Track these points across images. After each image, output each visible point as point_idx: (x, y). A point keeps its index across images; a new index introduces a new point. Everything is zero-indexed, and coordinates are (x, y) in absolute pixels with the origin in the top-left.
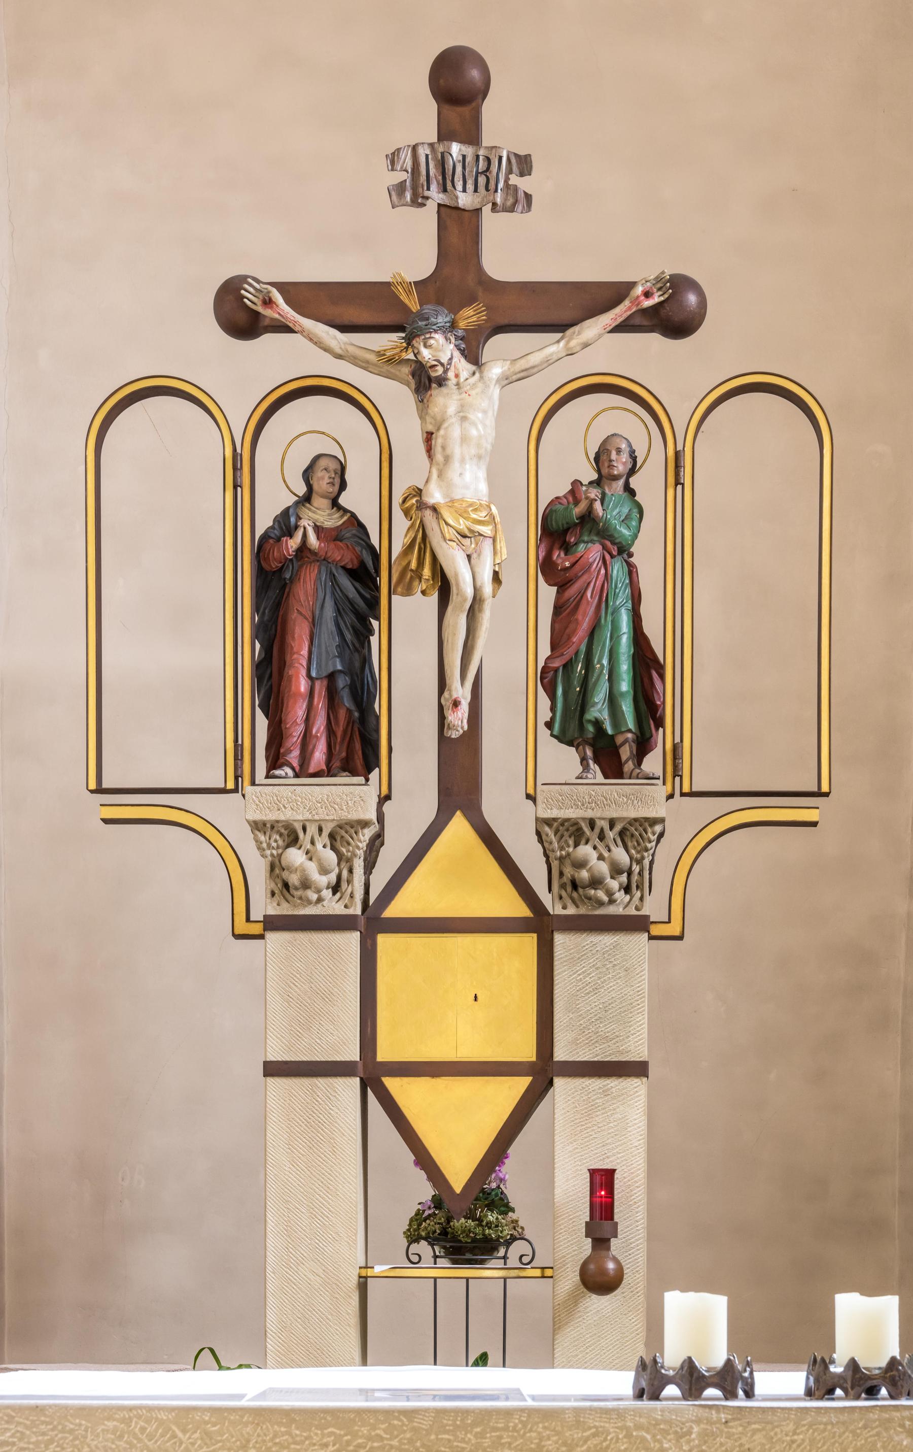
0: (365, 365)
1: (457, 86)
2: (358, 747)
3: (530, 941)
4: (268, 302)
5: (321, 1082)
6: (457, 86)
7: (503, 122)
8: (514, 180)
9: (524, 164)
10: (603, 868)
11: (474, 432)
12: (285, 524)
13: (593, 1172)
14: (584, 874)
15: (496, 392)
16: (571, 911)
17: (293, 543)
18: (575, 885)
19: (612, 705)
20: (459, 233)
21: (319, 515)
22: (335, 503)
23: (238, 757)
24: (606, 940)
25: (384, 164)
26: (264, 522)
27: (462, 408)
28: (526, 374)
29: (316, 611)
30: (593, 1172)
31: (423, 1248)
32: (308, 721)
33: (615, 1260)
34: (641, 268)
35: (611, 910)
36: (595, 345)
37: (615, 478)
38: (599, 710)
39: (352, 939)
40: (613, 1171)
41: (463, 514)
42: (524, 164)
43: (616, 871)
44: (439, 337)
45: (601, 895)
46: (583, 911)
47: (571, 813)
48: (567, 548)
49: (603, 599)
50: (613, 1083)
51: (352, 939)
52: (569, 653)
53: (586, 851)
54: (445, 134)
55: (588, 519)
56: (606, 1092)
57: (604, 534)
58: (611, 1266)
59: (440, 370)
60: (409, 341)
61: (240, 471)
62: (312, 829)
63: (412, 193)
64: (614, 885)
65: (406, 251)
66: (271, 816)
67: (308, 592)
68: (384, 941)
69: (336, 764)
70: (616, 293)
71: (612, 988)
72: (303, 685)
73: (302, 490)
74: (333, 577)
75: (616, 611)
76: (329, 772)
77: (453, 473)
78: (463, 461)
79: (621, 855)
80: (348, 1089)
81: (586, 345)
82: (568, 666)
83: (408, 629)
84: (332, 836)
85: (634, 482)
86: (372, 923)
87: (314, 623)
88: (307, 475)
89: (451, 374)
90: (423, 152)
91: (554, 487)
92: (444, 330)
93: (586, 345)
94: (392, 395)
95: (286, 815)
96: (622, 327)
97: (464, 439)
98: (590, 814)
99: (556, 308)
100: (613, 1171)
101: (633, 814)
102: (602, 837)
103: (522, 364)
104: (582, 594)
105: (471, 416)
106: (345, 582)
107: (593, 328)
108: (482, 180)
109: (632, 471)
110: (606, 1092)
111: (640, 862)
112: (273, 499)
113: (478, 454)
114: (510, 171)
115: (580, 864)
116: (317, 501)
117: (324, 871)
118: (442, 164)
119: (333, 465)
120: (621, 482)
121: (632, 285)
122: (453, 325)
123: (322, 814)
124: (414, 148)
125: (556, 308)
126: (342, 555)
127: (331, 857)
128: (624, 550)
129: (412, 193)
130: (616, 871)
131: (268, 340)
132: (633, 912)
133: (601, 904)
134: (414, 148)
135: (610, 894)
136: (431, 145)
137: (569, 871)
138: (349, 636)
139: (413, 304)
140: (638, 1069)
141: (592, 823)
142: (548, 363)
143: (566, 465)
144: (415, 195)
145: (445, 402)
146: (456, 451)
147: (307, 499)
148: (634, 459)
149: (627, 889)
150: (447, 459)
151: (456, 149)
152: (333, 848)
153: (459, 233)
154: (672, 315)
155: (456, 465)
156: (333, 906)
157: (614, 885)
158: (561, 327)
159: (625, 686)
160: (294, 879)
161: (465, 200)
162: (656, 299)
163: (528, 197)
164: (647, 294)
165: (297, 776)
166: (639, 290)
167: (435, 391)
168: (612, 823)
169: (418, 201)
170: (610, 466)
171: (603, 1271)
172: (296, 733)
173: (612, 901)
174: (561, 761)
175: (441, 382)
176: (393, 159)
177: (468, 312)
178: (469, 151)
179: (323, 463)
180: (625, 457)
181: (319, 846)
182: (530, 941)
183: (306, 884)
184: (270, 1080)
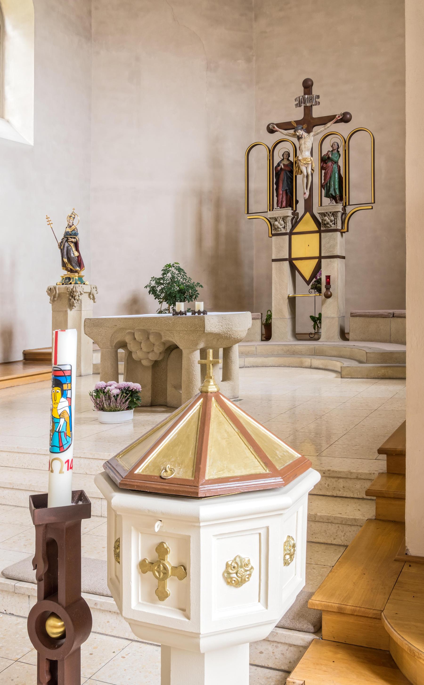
0: (290, 136)
1: (308, 86)
2: (290, 201)
3: (293, 256)
4: (274, 128)
5: (281, 262)
6: (308, 86)
7: (315, 91)
8: (317, 100)
9: (318, 97)
10: (329, 221)
11: (306, 146)
12: (279, 165)
13: (326, 276)
14: (326, 222)
15: (312, 138)
16: (324, 229)
17: (279, 168)
18: (325, 225)
19: (336, 188)
20: (308, 110)
21: (286, 162)
22: (288, 159)
23: (270, 206)
24: (330, 234)
25: (294, 100)
26: (275, 165)
27: (305, 142)
28: (318, 134)
29: (284, 177)
30: (326, 276)
31: (313, 291)
32: (282, 198)
33: (330, 292)
34: (338, 112)
35: (331, 228)
36: (331, 127)
37: (335, 150)
38: (332, 192)
39: (287, 237)
40: (330, 276)
41: (305, 160)
42: (318, 97)
43: (331, 221)
44: (300, 131)
45: (329, 226)
46: (326, 229)
47: (323, 212)
48: (326, 163)
49: (332, 171)
50: (332, 260)
51: (287, 237)
52: (326, 182)
53: (326, 218)
54: (305, 94)
55: (329, 158)
56: (330, 261)
57: (332, 160)
58: (329, 293)
59: (300, 136)
60: (295, 131)
61: (271, 152)
62: (279, 218)
63: (298, 105)
64: (331, 224)
65: (298, 114)
66: (272, 216)
67: (283, 175)
68: (293, 236)
69: (288, 205)
70: (334, 117)
71: (337, 243)
72: (281, 192)
73: (282, 158)
74: (287, 173)
75: (335, 173)
76: (286, 207)
77: (303, 153)
78: (305, 151)
79: (332, 218)
80: (287, 263)
81: (328, 127)
82: (327, 184)
83: (300, 180)
84: (283, 219)
85: (339, 150)
86: (291, 234)
87: (283, 181)
88: (283, 155)
89: (303, 136)
90: (301, 98)
91: (324, 153)
92: (301, 130)
93: (328, 127)
94: (295, 140)
95: (274, 216)
96: (336, 122)
97: (305, 147)
98: (326, 211)
99: (324, 121)
100: (330, 276)
101: (334, 211)
102: (329, 215)
103: (317, 132)
104: (328, 171)
105: (306, 143)
106: (288, 173)
107: (329, 124)
108: (311, 101)
109: (338, 148)
110: (330, 261)
111: (336, 219)
112: (277, 159)
113: (308, 149)
114: (316, 98)
115: (325, 220)
116: (285, 160)
117: (281, 225)
118: (304, 99)
119: (287, 153)
120: (336, 150)
121: (336, 115)
122: (302, 128)
123: (280, 215)
124: (299, 97)
125: (324, 121)
126: (287, 169)
127: (282, 222)
128: (336, 163)
129: (298, 105)
130: (331, 221)
131: (276, 133)
132: (335, 228)
133: (279, 231)
134: (299, 97)
135: (330, 225)
136: (302, 96)
137: (323, 222)
138: (289, 183)
139: (296, 126)
140: (274, 260)
141: (327, 213)
142: (321, 131)
143: (327, 148)
144: (299, 105)
145: (302, 141)
146: (304, 149)
147: (283, 159)
148: (338, 146)
149: (334, 224)
150: (302, 151)
151: (306, 96)
152: (283, 221)
153: (308, 110)
154: (345, 118)
155: (304, 152)
156: (283, 231)
157: (331, 224)
158: (325, 124)
159: (337, 187)
160: (276, 227)
161: (308, 105)
162: (341, 117)
163: (319, 102)
164: (339, 117)
165: (280, 208)
166: (337, 116)
167: (301, 139)
168: (330, 212)
169: (300, 106)
170: (335, 149)
171: (327, 294)
172: (280, 201)
173: (331, 227)
174: (326, 201)
175: (301, 138)
176: (296, 100)
177: (304, 126)
178: (309, 96)
179: (285, 153)
180: (336, 146)
181: (280, 221)
182: (293, 256)
183: (278, 228)
184: (273, 263)
